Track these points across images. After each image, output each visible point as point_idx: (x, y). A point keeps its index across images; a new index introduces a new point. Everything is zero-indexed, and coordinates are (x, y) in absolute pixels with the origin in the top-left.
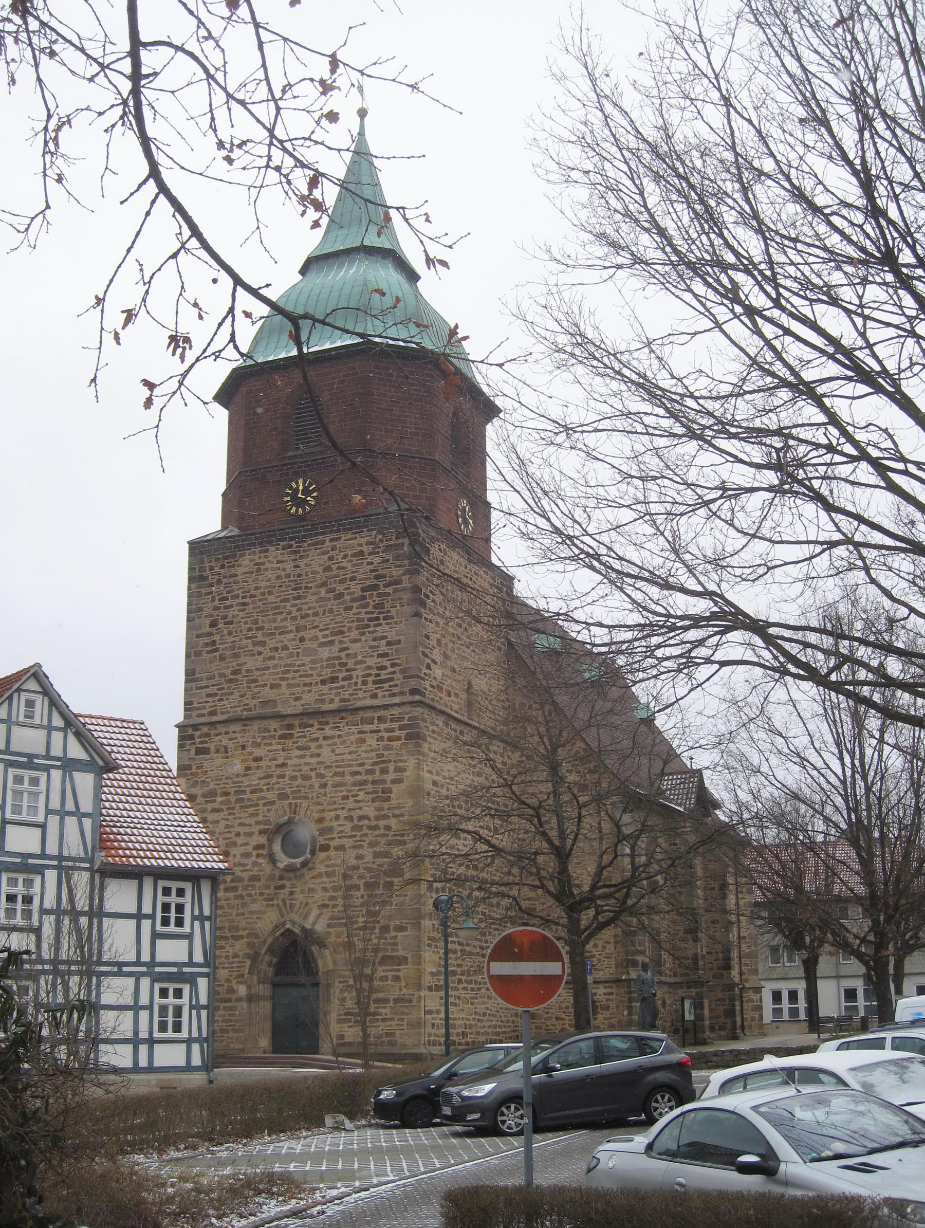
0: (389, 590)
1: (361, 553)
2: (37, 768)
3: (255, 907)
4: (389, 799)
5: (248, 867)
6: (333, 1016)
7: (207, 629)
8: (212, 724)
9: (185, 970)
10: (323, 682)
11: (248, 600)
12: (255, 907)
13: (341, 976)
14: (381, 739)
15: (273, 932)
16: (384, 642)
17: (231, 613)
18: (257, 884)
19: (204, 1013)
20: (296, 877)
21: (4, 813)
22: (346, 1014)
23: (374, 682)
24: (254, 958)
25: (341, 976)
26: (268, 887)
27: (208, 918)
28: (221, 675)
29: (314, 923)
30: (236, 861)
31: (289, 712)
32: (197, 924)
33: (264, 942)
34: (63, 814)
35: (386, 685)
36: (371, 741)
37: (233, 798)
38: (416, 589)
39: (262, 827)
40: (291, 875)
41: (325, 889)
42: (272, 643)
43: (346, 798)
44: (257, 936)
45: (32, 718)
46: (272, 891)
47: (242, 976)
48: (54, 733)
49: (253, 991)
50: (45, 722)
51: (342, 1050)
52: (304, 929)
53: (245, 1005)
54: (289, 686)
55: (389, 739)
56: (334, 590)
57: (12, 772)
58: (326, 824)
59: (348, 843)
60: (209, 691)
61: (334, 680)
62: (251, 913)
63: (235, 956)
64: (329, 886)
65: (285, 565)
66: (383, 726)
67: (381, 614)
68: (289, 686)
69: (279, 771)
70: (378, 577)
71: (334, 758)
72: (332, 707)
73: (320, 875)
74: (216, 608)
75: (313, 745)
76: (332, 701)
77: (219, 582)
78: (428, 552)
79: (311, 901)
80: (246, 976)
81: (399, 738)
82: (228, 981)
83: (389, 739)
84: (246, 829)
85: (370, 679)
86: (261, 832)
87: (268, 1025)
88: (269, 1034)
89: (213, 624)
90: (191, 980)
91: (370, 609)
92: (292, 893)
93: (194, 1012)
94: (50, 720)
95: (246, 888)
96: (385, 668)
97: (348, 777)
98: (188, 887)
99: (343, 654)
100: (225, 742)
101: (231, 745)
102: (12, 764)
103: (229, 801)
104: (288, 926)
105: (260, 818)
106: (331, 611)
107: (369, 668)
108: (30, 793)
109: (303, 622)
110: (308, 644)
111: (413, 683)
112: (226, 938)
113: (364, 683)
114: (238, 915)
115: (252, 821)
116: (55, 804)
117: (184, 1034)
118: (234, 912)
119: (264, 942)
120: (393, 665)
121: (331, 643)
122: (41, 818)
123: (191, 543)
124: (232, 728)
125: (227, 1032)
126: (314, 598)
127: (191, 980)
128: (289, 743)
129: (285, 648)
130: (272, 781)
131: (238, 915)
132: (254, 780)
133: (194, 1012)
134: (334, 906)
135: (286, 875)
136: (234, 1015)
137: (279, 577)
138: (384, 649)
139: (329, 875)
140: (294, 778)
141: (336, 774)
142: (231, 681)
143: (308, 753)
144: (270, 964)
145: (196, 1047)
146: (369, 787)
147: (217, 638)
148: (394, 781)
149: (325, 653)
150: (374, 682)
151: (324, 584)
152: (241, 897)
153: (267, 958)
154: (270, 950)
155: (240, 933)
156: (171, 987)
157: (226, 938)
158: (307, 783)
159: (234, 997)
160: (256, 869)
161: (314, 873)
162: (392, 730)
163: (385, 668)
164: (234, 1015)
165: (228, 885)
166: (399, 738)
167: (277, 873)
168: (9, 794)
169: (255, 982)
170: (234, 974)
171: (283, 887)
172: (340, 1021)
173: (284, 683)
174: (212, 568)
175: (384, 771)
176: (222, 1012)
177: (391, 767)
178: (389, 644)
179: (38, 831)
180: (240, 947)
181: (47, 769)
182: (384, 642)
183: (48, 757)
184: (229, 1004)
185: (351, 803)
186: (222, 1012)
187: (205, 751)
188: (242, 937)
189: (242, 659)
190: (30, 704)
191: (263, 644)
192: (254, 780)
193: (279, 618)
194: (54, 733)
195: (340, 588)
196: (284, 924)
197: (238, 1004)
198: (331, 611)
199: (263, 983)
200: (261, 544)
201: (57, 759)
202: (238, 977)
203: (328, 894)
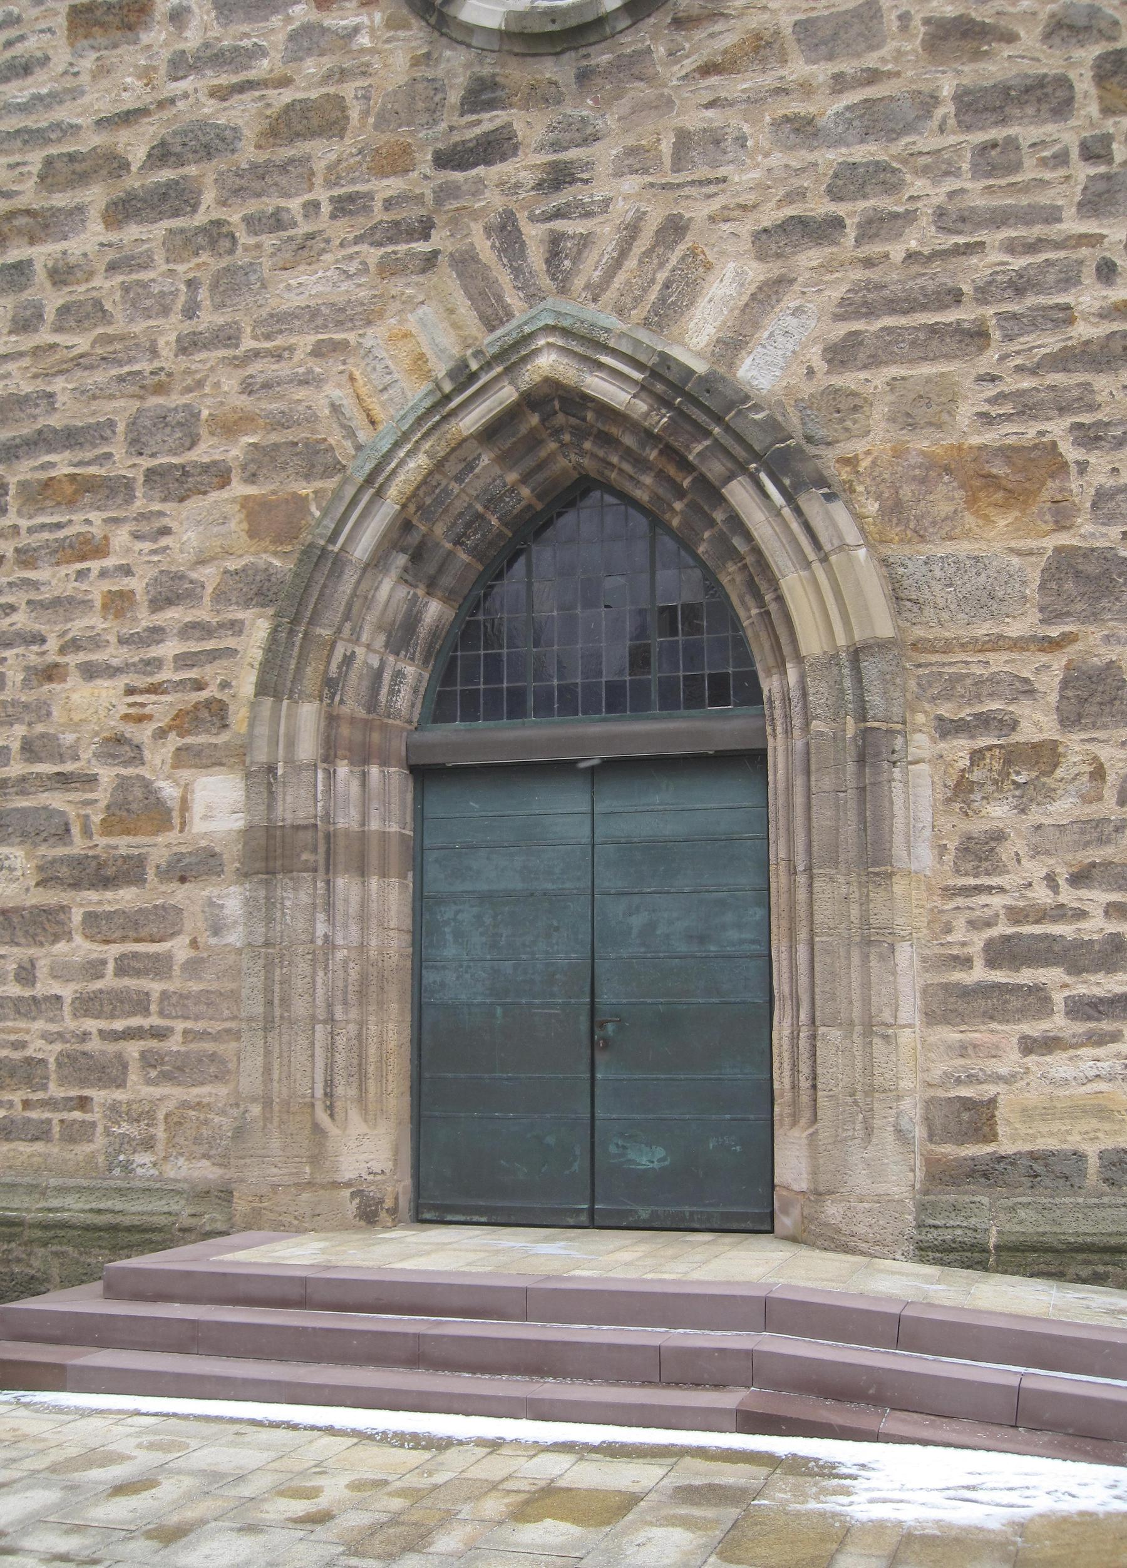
3: (310, 285)
5: (262, 68)
6: (907, 976)
12: (310, 285)
13: (950, 687)
15: (441, 409)
18: (323, 152)
20: (584, 76)
22: (1002, 953)
24: (300, 598)
25: (950, 687)
26: (395, 161)
29: (732, 345)
30: (192, 40)
33: (375, 481)
40: (555, 70)
41: (803, 130)
44: (315, 459)
46: (422, 178)
47: (216, 713)
49: (295, 805)
51: (993, 1218)
52: (663, 379)
53: (233, 899)
62: (281, 321)
63: (171, 591)
64: (828, 108)
72: (813, 783)
73: (762, 47)
79: (698, 211)
80: (239, 717)
82: (118, 747)
87: (390, 1032)
88: (394, 1092)
92: (559, 177)
104: (547, 363)
112: (115, 490)
114: (188, 345)
118: (170, 330)
119: (375, 481)
125: (110, 1073)
131: (188, 345)
134: (876, 226)
135: (517, 74)
136: (159, 966)
144: (402, 634)
152: (216, 235)
153: (389, 591)
154: (408, 541)
155: (205, 451)
157: (115, 490)
159: (159, 848)
160: (311, 66)
164: (159, 966)
165: (133, 182)
167: (456, 67)
169: (307, 748)
170: (162, 707)
171: (495, 147)
172: (951, 1004)
176: (79, 947)
180: (204, 533)
184: (126, 897)
186: (79, 947)
188: (220, 475)
196: (512, 355)
197: (187, 897)
199: (362, 757)
202: (187, 721)
203: (830, 157)
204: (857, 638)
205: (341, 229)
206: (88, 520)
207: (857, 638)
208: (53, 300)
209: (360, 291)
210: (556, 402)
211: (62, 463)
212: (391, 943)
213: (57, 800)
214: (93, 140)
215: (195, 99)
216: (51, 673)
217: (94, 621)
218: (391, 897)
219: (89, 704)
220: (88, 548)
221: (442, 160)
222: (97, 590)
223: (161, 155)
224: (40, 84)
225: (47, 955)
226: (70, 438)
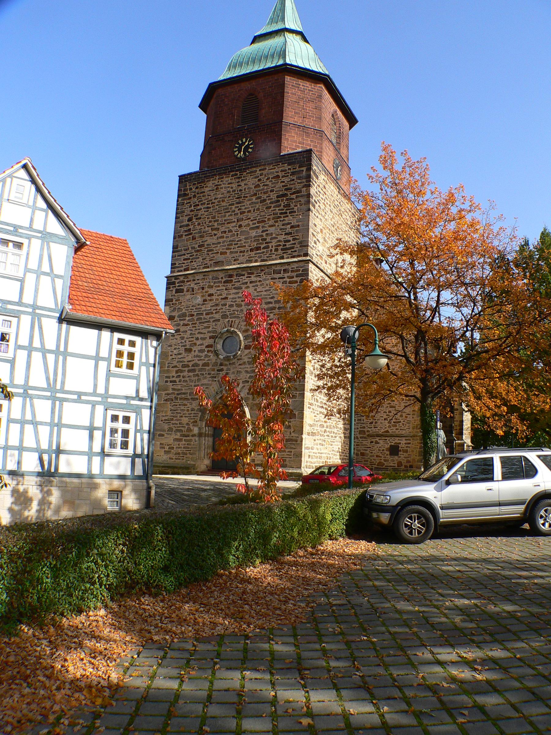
0: (294, 196)
1: (278, 177)
3: (205, 381)
10: (251, 250)
16: (289, 226)
18: (207, 368)
19: (146, 436)
23: (282, 250)
26: (213, 370)
30: (196, 354)
32: (144, 369)
35: (289, 251)
42: (223, 229)
50: (31, 203)
55: (290, 283)
60: (185, 257)
61: (258, 248)
65: (233, 185)
69: (223, 302)
74: (192, 211)
77: (195, 196)
78: (317, 178)
81: (296, 282)
82: (188, 424)
83: (290, 283)
84: (202, 336)
85: (280, 248)
91: (282, 207)
93: (138, 435)
94: (35, 202)
95: (200, 370)
96: (289, 241)
99: (264, 234)
100: (192, 286)
101: (196, 287)
103: (193, 320)
105: (210, 329)
107: (280, 241)
110: (244, 229)
113: (276, 250)
115: (205, 331)
120: (294, 239)
121: (258, 227)
129: (230, 231)
132: (208, 306)
133: (138, 435)
136: (190, 444)
137: (229, 192)
138: (289, 230)
140: (231, 306)
142: (198, 251)
149: (253, 233)
150: (282, 250)
151: (255, 194)
152: (197, 375)
158: (239, 309)
162: (293, 277)
163: (289, 241)
164: (190, 444)
166: (296, 282)
170: (192, 421)
171: (222, 370)
173: (228, 251)
174: (191, 189)
178: (292, 227)
182: (289, 226)
184: (188, 438)
186: (184, 442)
187: (181, 291)
191: (218, 229)
192: (208, 306)
193: (227, 214)
198: (258, 209)
201: (39, 232)
202: (193, 422)
205: (208, 376)
206: (185, 402)
208: (183, 379)
209: (210, 382)
211: (183, 396)
212: (211, 443)
213: (182, 429)
214: (186, 363)
215: (196, 360)
216: (182, 417)
217: (186, 412)
218: (211, 439)
219: (185, 420)
220: (185, 405)
221: (218, 370)
222: (186, 409)
223: (193, 366)
224: (182, 356)
225: (181, 443)
226: (184, 394)
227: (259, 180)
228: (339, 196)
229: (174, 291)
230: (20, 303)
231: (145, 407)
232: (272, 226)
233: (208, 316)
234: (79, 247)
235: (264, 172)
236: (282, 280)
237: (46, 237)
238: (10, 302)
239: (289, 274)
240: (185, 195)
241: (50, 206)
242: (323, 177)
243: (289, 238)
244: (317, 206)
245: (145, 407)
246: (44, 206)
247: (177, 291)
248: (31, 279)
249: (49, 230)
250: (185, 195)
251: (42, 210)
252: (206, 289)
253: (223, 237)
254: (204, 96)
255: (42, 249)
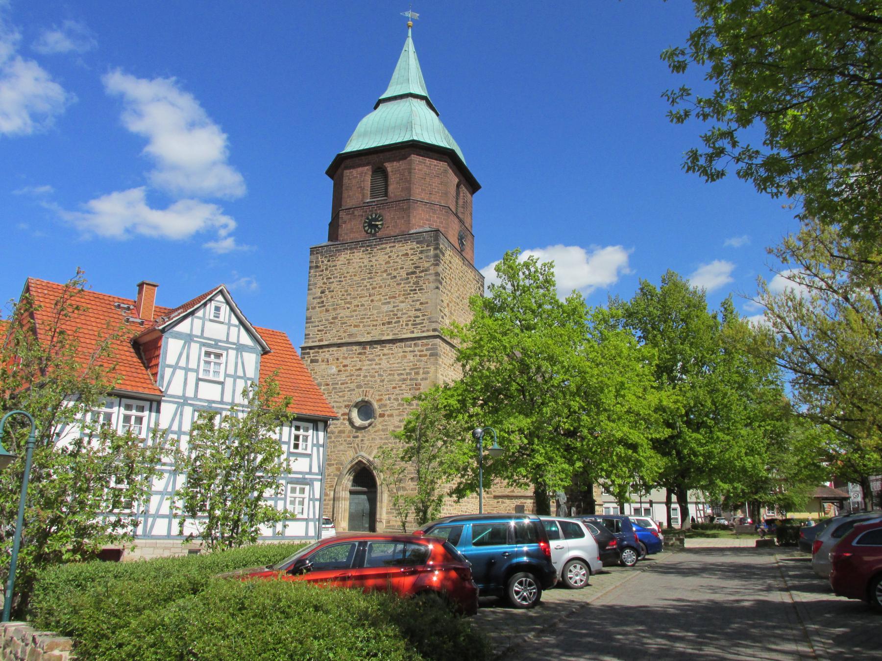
0: (423, 274)
1: (407, 254)
2: (220, 348)
3: (342, 447)
4: (419, 389)
7: (319, 294)
8: (321, 347)
9: (307, 476)
10: (383, 324)
11: (343, 279)
12: (342, 447)
14: (415, 356)
16: (418, 303)
17: (333, 286)
18: (343, 435)
19: (317, 503)
21: (198, 374)
23: (413, 325)
26: (349, 437)
27: (321, 446)
28: (326, 320)
31: (364, 340)
32: (315, 449)
34: (235, 377)
35: (419, 327)
36: (410, 357)
37: (331, 387)
38: (437, 274)
39: (347, 403)
41: (381, 439)
42: (356, 303)
43: (395, 388)
45: (218, 317)
48: (232, 328)
50: (227, 321)
52: (369, 461)
54: (364, 326)
55: (420, 356)
56: (390, 274)
57: (204, 349)
58: (383, 402)
59: (395, 412)
60: (319, 328)
61: (389, 323)
65: (364, 260)
66: (416, 349)
67: (418, 288)
68: (364, 326)
69: (357, 373)
70: (416, 267)
71: (389, 366)
74: (324, 283)
75: (377, 359)
76: (388, 334)
77: (327, 269)
78: (443, 255)
81: (426, 355)
83: (420, 356)
84: (338, 404)
85: (410, 323)
86: (346, 406)
87: (347, 515)
89: (322, 292)
90: (310, 483)
91: (411, 284)
92: (362, 440)
93: (311, 503)
94: (229, 320)
95: (336, 437)
96: (418, 317)
97: (396, 376)
98: (311, 425)
99: (395, 309)
100: (327, 356)
101: (331, 359)
102: (204, 345)
103: (328, 389)
105: (346, 398)
106: (389, 285)
107: (410, 317)
108: (215, 363)
109: (372, 291)
110: (376, 303)
111: (434, 326)
113: (407, 325)
115: (341, 400)
116: (231, 371)
117: (305, 516)
120: (423, 315)
121: (389, 303)
122: (222, 380)
123: (327, 173)
124: (331, 349)
126: (380, 278)
127: (310, 483)
128: (363, 357)
129: (362, 305)
130: (354, 378)
132: (343, 377)
133: (311, 503)
137: (360, 267)
138: (418, 306)
139: (383, 430)
140: (365, 376)
141: (390, 374)
142: (331, 323)
143: (374, 363)
145: (311, 524)
146: (408, 382)
147: (324, 299)
148: (422, 379)
149: (385, 308)
150: (413, 325)
151: (386, 271)
156: (298, 487)
158: (373, 379)
161: (376, 429)
162: (422, 351)
163: (418, 317)
166: (426, 355)
168: (202, 363)
173: (361, 325)
174: (323, 262)
175: (417, 373)
177: (421, 371)
178: (421, 304)
179: (220, 387)
181: (227, 349)
182: (418, 303)
183: (227, 342)
185: (397, 391)
187: (316, 361)
189: (338, 311)
190: (217, 309)
191: (350, 303)
192: (343, 377)
193: (360, 289)
194: (232, 328)
195: (394, 273)
196: (357, 457)
198: (389, 285)
200: (351, 249)
201: (234, 344)
204: (532, 494)
207: (532, 494)
210: (360, 461)
227: (389, 257)
228: (464, 267)
229: (309, 361)
230: (222, 402)
231: (316, 480)
232: (403, 302)
233: (343, 386)
234: (265, 352)
235: (394, 250)
236: (412, 354)
237: (240, 348)
238: (214, 402)
239: (420, 348)
240: (317, 267)
241: (241, 323)
242: (448, 252)
243: (418, 313)
244: (444, 284)
245: (316, 480)
246: (236, 322)
247: (312, 361)
248: (229, 382)
249: (241, 342)
250: (317, 267)
251: (236, 326)
252: (341, 360)
253: (355, 311)
254: (333, 163)
255: (237, 358)
